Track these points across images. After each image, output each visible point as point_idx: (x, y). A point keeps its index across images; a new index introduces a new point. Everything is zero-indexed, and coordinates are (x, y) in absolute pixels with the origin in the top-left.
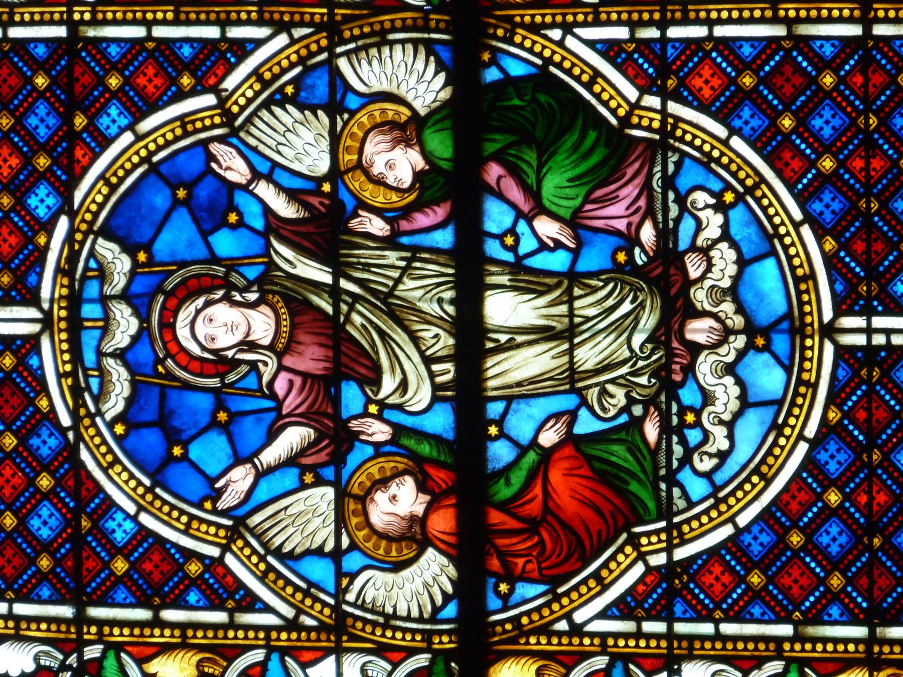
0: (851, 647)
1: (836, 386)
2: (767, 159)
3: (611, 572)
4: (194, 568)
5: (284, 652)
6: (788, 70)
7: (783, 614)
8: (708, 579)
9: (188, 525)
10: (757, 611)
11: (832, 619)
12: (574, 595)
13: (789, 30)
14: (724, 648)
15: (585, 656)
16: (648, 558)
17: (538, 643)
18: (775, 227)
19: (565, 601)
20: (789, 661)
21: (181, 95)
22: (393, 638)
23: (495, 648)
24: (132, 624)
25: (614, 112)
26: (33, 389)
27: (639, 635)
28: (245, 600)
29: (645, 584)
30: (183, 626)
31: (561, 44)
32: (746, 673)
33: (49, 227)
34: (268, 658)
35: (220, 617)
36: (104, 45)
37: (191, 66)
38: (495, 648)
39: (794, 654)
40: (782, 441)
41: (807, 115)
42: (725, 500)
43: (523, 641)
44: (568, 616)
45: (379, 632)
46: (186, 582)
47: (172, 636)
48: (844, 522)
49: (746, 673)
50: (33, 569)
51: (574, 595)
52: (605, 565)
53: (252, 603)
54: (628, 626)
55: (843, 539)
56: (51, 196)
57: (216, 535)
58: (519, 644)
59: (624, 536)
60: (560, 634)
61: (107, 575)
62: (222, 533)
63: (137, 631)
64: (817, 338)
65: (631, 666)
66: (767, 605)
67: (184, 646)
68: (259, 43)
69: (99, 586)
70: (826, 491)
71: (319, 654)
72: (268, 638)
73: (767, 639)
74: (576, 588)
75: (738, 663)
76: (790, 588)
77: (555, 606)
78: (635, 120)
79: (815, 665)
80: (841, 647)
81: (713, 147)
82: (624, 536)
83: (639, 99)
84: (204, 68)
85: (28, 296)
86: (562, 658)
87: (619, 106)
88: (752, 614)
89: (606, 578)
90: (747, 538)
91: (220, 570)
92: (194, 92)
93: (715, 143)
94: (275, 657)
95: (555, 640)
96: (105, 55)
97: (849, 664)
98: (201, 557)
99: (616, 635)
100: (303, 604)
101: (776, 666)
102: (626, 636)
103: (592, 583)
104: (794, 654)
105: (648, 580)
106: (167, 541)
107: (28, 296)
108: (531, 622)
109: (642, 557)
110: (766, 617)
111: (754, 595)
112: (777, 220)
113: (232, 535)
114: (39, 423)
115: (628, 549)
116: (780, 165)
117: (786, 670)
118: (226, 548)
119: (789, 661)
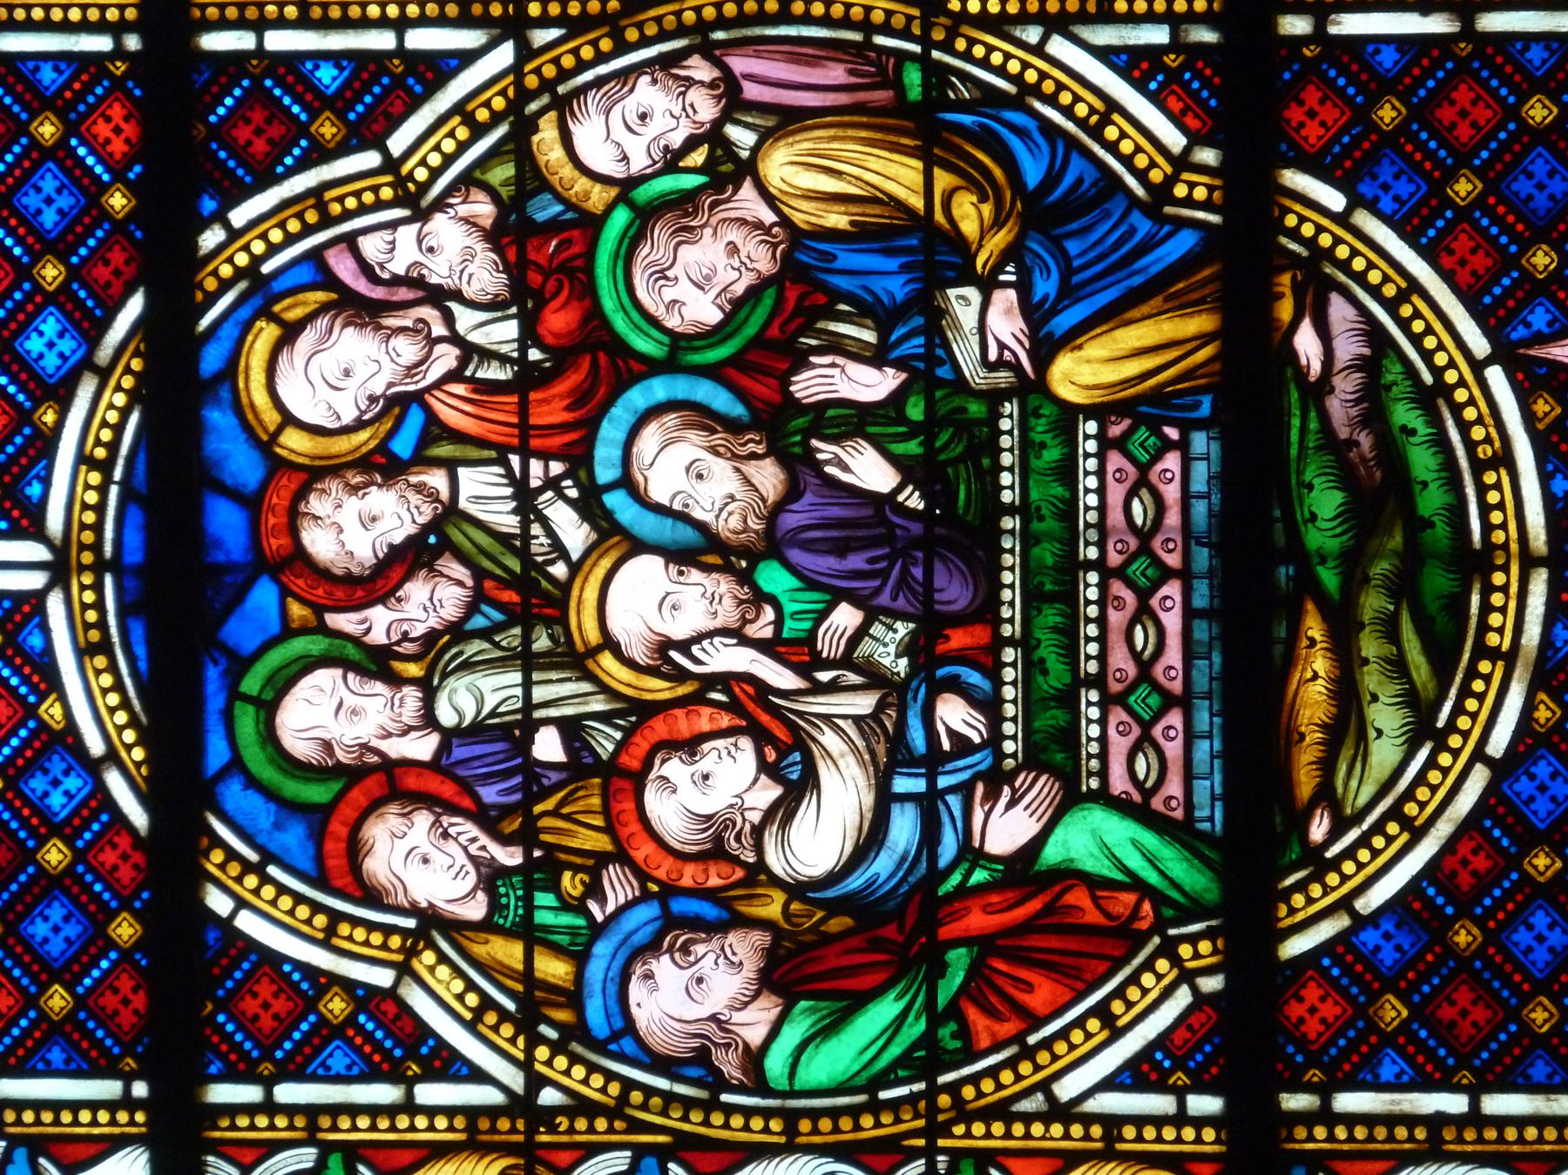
0: (1531, 1133)
1: (1549, 659)
2: (1429, 254)
3: (1130, 1005)
6: (276, 131)
7: (102, 1062)
8: (250, 1005)
10: (339, 1063)
11: (333, 1072)
12: (1060, 1048)
13: (1174, 34)
14: (836, 1130)
15: (272, 1148)
17: (988, 1135)
18: (1438, 372)
19: (1043, 1057)
20: (326, 1149)
21: (320, 154)
22: (354, 1128)
23: (906, 1143)
25: (1141, 175)
26: (34, 689)
27: (1181, 1118)
29: (397, 1017)
31: (1038, 50)
32: (246, 1170)
33: (62, 395)
35: (384, 1093)
36: (309, 66)
37: (337, 104)
38: (906, 1143)
40: (1445, 759)
41: (85, 211)
43: (959, 1130)
45: (1470, 1135)
46: (1526, 1042)
48: (74, 900)
49: (246, 1170)
50: (312, 1018)
51: (1060, 1048)
52: (1119, 993)
53: (448, 1065)
54: (1162, 1104)
55: (72, 930)
56: (67, 335)
58: (953, 1136)
59: (1157, 940)
61: (312, 1025)
64: (1515, 569)
65: (42, 1161)
66: (75, 1046)
68: (467, 58)
70: (44, 844)
72: (313, 1128)
73: (1411, 1120)
74: (1063, 1034)
76: (256, 1018)
77: (1025, 1068)
78: (1180, 191)
80: (1360, 1132)
81: (1320, 229)
82: (1157, 940)
83: (1187, 150)
84: (1485, 74)
85: (25, 522)
87: (1153, 164)
88: (48, 1063)
89: (1119, 1017)
90: (1370, 937)
91: (390, 1008)
93: (1325, 222)
95: (1018, 1129)
96: (33, 86)
97: (439, 1151)
98: (349, 986)
99: (1140, 1121)
100: (1023, 1078)
101: (306, 1157)
102: (1159, 1121)
103: (1093, 1025)
104: (496, 1138)
105: (1194, 1021)
107: (25, 522)
108: (980, 1095)
109: (1187, 977)
110: (73, 1066)
111: (52, 1029)
112: (1441, 359)
113: (415, 944)
114: (45, 752)
115: (1162, 965)
116: (1447, 262)
117: (321, 1163)
118: (404, 970)
119: (326, 1149)
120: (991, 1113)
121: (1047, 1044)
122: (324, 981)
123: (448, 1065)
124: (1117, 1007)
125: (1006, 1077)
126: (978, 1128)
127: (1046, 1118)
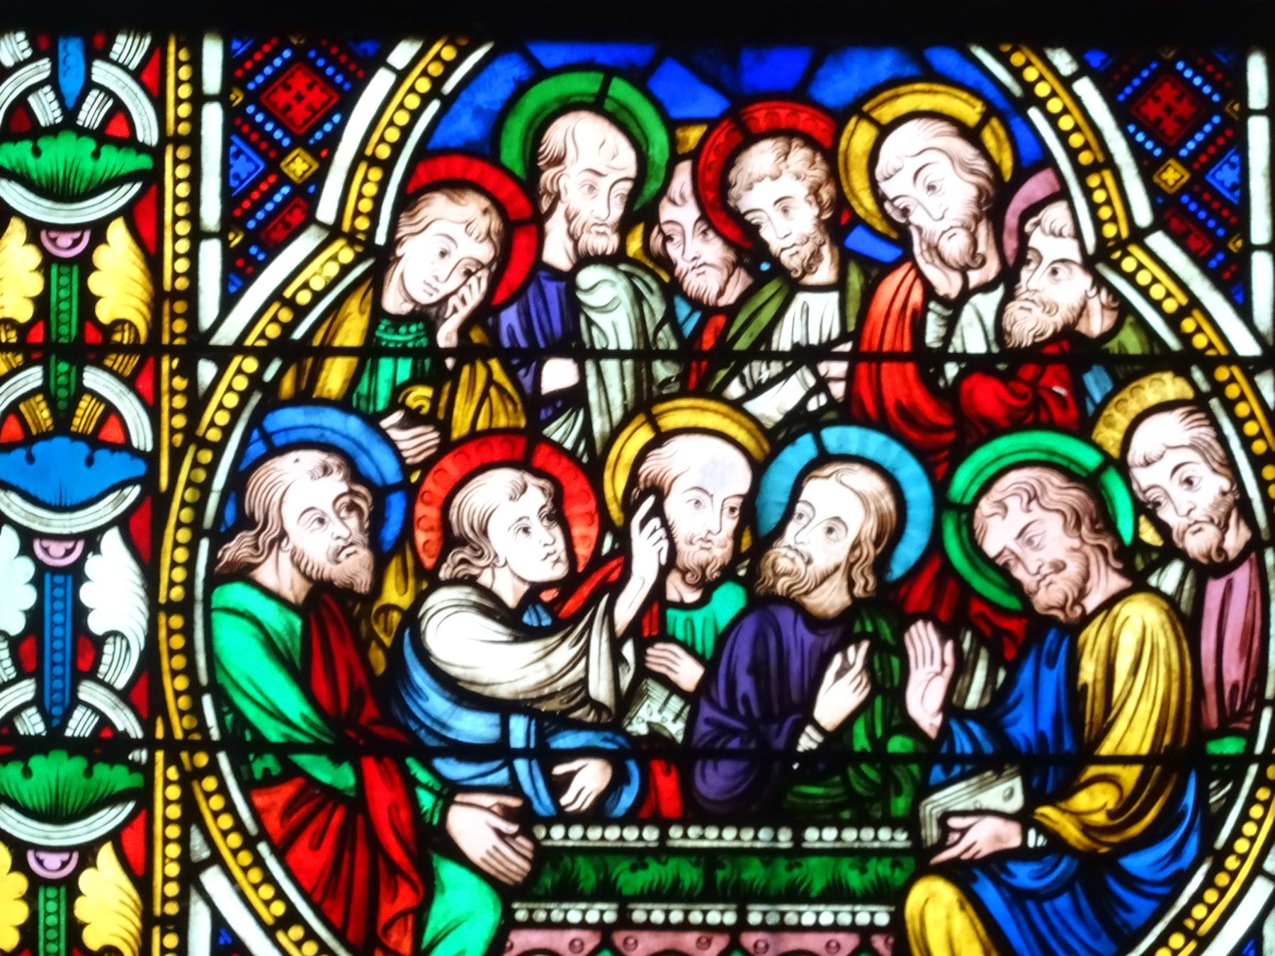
4: (298, 165)
5: (148, 481)
9: (374, 161)
10: (241, 166)
11: (232, 161)
16: (325, 235)
21: (1148, 168)
24: (194, 199)
28: (246, 71)
30: (194, 140)
34: (142, 148)
35: (211, 214)
37: (1198, 185)
39: (166, 319)
42: (426, 99)
44: (216, 858)
47: (165, 899)
53: (239, 272)
57: (357, 213)
60: (184, 841)
62: (362, 224)
63: (182, 209)
67: (148, 920)
69: (268, 60)
71: (150, 399)
72: (178, 141)
74: (269, 878)
75: (157, 55)
77: (235, 840)
79: (140, 822)
86: (157, 55)
92: (1153, 190)
94: (145, 162)
98: (319, 178)
103: (279, 908)
106: (346, 112)
118: (334, 232)
120: (188, 802)
121: (259, 861)
122: (324, 153)
123: (239, 272)
124: (296, 932)
125: (226, 821)
126: (174, 792)
127: (184, 859)
